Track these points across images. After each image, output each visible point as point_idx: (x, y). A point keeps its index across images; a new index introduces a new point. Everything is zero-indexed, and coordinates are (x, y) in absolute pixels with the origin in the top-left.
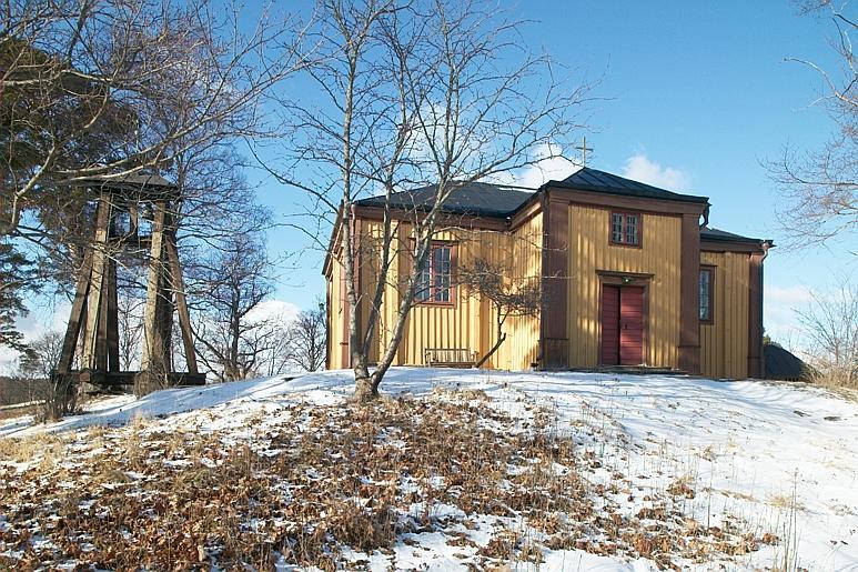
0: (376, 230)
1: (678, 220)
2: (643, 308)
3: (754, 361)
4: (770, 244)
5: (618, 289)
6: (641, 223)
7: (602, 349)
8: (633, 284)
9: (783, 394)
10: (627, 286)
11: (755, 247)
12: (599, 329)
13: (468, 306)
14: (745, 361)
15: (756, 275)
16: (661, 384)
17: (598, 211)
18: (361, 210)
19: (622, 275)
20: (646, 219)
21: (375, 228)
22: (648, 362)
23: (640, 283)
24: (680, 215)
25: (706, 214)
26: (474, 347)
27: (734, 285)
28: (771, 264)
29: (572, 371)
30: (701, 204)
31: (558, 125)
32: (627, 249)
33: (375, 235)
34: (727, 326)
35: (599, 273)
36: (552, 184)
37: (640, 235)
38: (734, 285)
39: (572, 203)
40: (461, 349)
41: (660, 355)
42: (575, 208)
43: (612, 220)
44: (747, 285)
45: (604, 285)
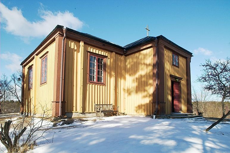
21: (73, 44)
26: (112, 102)
33: (72, 47)
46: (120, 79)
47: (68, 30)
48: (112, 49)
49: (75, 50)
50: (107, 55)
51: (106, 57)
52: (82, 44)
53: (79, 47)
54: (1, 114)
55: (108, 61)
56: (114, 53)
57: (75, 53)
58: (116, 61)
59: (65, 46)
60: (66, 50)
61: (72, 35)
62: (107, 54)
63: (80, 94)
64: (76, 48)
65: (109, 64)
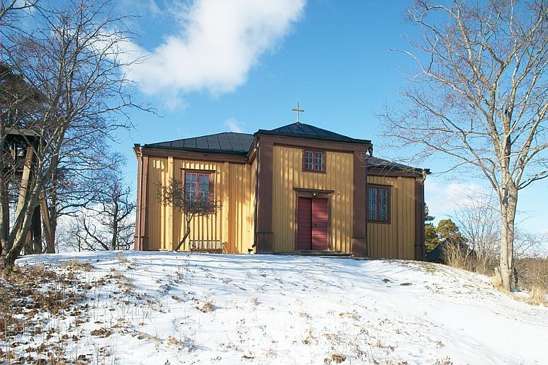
0: (158, 164)
1: (352, 155)
2: (327, 209)
3: (418, 248)
4: (428, 171)
5: (310, 200)
6: (325, 159)
7: (299, 234)
8: (319, 197)
9: (448, 276)
10: (316, 199)
11: (417, 175)
12: (296, 227)
13: (216, 217)
14: (413, 247)
15: (420, 190)
16: (337, 264)
17: (295, 150)
18: (147, 151)
19: (311, 191)
20: (329, 155)
21: (158, 162)
22: (330, 247)
23: (325, 196)
24: (353, 152)
25: (370, 149)
26: (225, 239)
27: (405, 196)
28: (429, 184)
29: (274, 254)
30: (367, 145)
31: (227, 282)
32: (316, 174)
33: (158, 167)
34: (400, 225)
35: (297, 190)
36: (261, 132)
37: (324, 166)
38: (405, 196)
39: (275, 144)
40: (216, 240)
41: (339, 243)
42: (278, 148)
43: (304, 151)
44: (413, 198)
45: (299, 197)
46: (240, 204)
47: (146, 146)
48: (221, 157)
49: (163, 170)
50: (215, 169)
51: (210, 172)
52: (170, 160)
53: (166, 165)
54: (513, 2)
55: (217, 178)
56: (226, 164)
57: (163, 173)
58: (230, 178)
59: (145, 177)
60: (147, 183)
61: (154, 151)
62: (215, 167)
63: (169, 227)
64: (163, 167)
65: (219, 181)
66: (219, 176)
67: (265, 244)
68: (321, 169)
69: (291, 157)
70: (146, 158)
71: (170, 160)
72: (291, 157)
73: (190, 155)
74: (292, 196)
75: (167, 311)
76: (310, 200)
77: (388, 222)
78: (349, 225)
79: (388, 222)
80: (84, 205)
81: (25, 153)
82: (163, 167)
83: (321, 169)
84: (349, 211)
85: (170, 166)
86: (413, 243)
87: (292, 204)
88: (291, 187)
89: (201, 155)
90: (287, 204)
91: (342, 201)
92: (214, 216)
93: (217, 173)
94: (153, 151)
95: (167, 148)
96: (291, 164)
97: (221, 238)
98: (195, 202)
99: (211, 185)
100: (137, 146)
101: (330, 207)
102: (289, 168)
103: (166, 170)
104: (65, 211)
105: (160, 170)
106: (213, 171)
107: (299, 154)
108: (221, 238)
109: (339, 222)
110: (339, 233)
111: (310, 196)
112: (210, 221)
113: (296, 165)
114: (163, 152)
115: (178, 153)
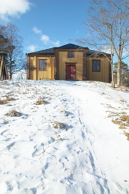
0: (32, 58)
2: (75, 68)
3: (110, 79)
5: (70, 66)
7: (66, 75)
8: (72, 65)
18: (29, 55)
33: (32, 59)
35: (66, 63)
39: (59, 51)
42: (61, 52)
48: (49, 55)
52: (35, 57)
53: (34, 58)
60: (29, 73)
64: (33, 59)
66: (48, 60)
67: (57, 77)
68: (73, 56)
69: (64, 54)
70: (29, 57)
71: (35, 57)
72: (64, 54)
73: (40, 55)
74: (65, 65)
75: (64, 180)
76: (70, 66)
77: (100, 71)
78: (81, 73)
79: (100, 71)
80: (19, 71)
81: (2, 58)
82: (33, 59)
83: (73, 56)
84: (82, 69)
85: (35, 59)
86: (108, 77)
87: (65, 68)
88: (64, 62)
89: (43, 55)
90: (63, 68)
91: (80, 65)
92: (46, 72)
93: (48, 60)
94: (31, 55)
95: (34, 54)
96: (64, 56)
97: (49, 77)
98: (42, 67)
99: (46, 64)
100: (26, 54)
101: (76, 68)
102: (64, 57)
103: (34, 60)
104: (14, 72)
105: (33, 60)
106: (47, 59)
107: (66, 53)
108: (49, 77)
109: (78, 72)
110: (78, 75)
111: (70, 65)
112: (46, 72)
113: (66, 56)
114: (33, 55)
115: (37, 55)
